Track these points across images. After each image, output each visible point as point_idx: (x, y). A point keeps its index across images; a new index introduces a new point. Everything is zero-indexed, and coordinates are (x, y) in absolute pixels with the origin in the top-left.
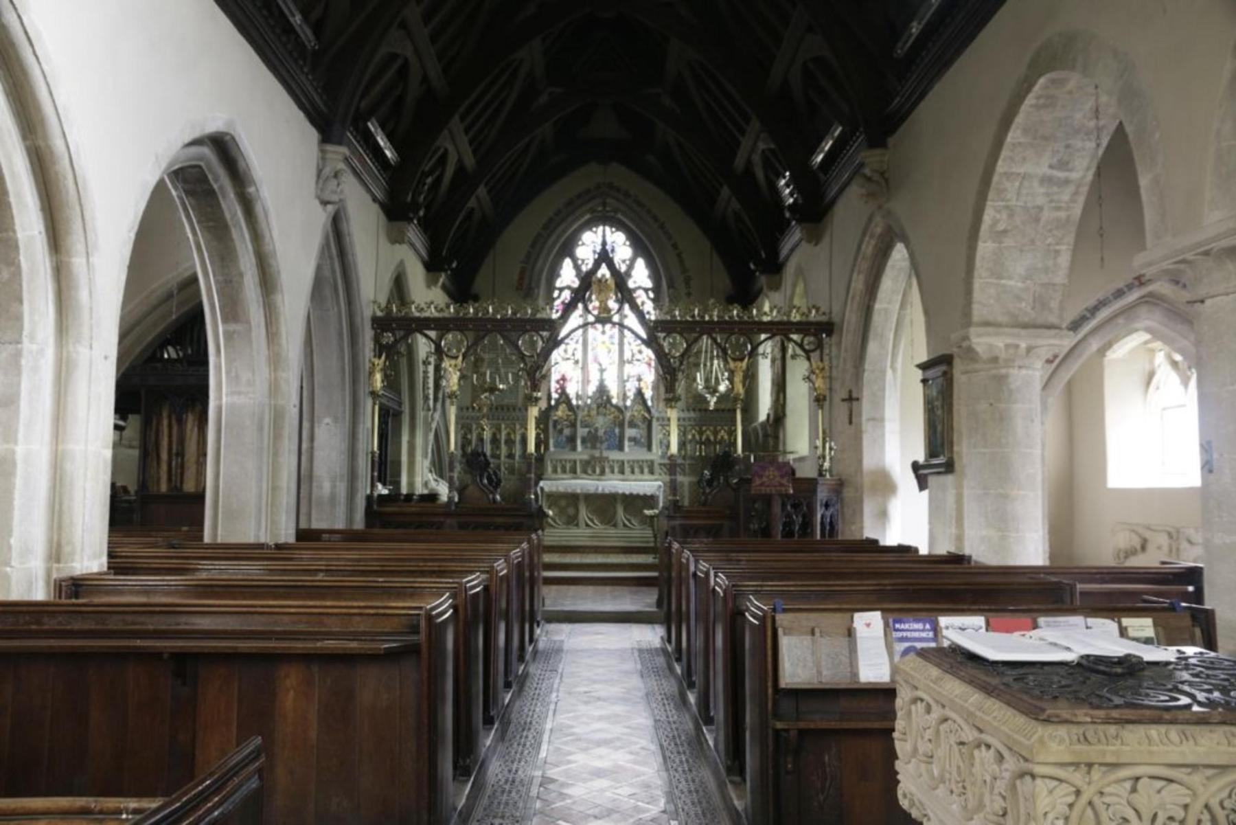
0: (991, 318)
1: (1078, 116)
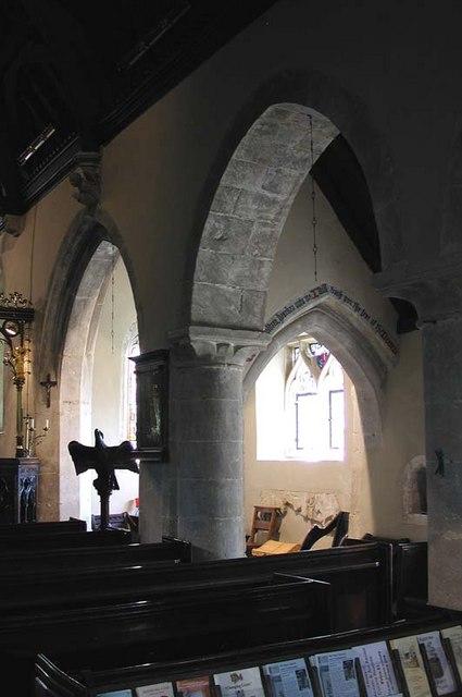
0: (207, 319)
1: (291, 146)
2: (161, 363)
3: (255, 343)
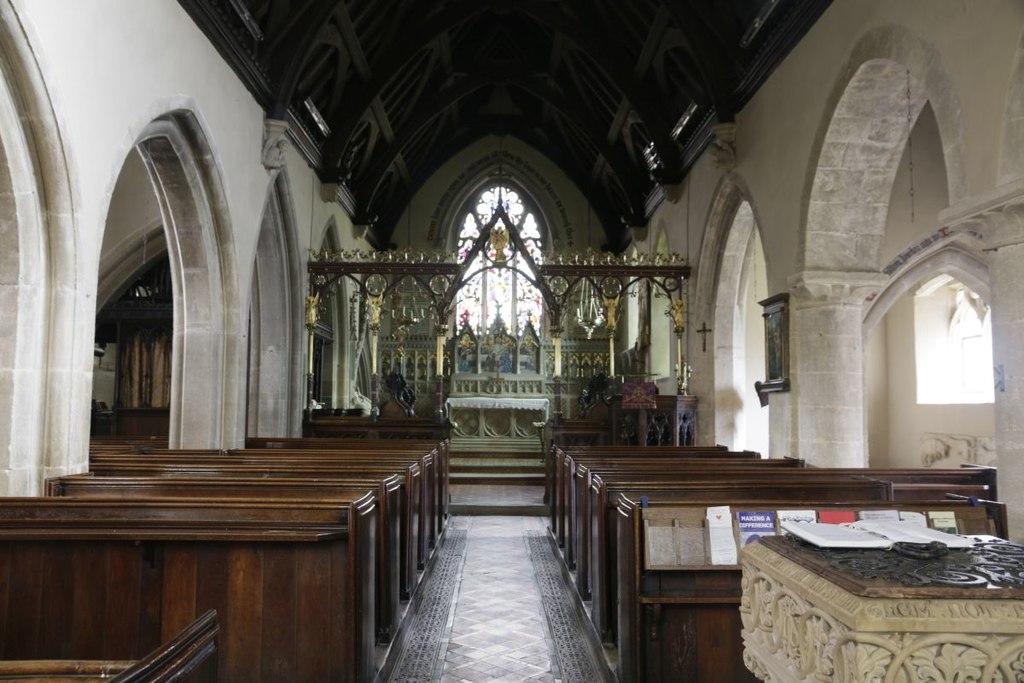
0: (820, 264)
2: (782, 305)
3: (871, 283)
